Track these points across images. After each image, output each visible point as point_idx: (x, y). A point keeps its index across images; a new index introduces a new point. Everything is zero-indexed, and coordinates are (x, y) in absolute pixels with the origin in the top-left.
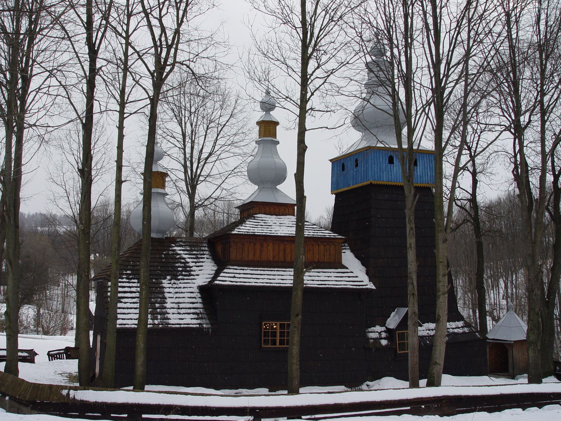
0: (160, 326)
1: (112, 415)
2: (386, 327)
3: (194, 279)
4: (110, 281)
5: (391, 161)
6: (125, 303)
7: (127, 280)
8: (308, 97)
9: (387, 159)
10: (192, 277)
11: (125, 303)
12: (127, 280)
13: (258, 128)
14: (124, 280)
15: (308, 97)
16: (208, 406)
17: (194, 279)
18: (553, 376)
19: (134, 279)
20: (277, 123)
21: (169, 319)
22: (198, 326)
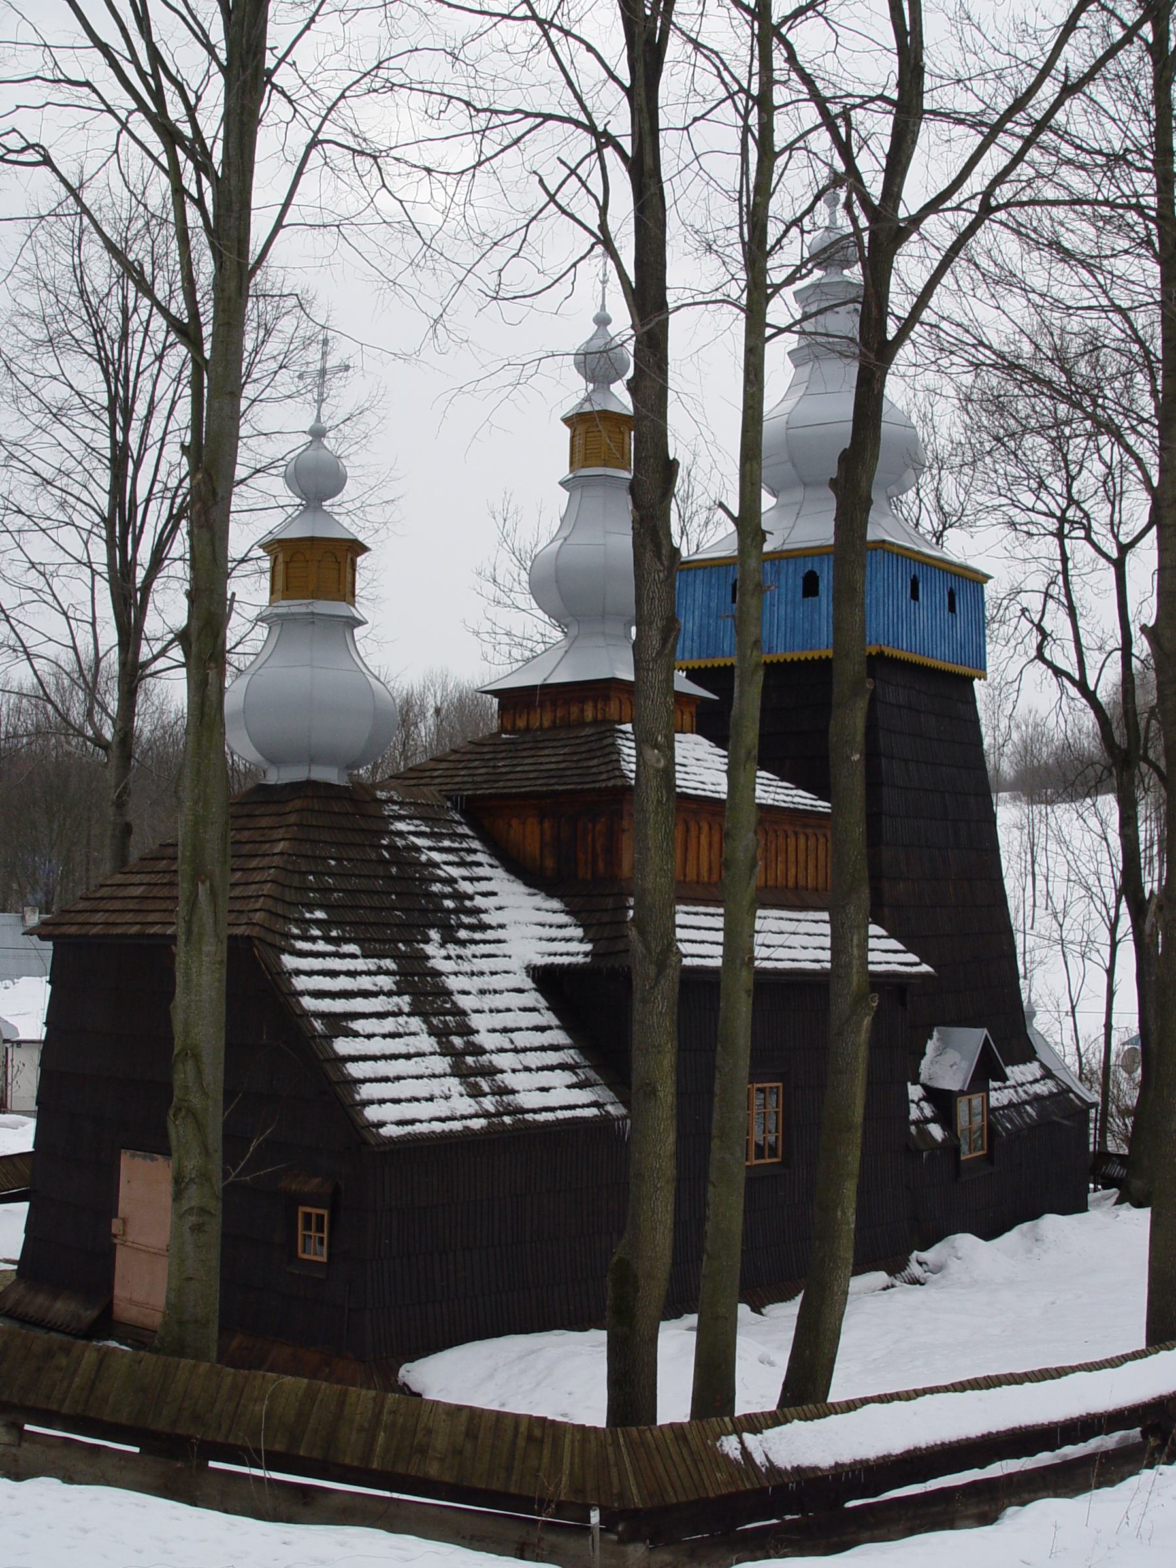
0: (507, 1119)
1: (212, 1464)
2: (924, 1086)
3: (499, 941)
4: (631, 895)
5: (810, 585)
6: (369, 1036)
7: (330, 948)
8: (944, 206)
9: (800, 582)
10: (490, 935)
11: (369, 1036)
12: (330, 948)
13: (567, 432)
14: (321, 946)
15: (944, 206)
16: (846, 1458)
17: (499, 941)
18: (1128, 1204)
19: (348, 941)
20: (357, 548)
21: (513, 1092)
22: (593, 1111)
